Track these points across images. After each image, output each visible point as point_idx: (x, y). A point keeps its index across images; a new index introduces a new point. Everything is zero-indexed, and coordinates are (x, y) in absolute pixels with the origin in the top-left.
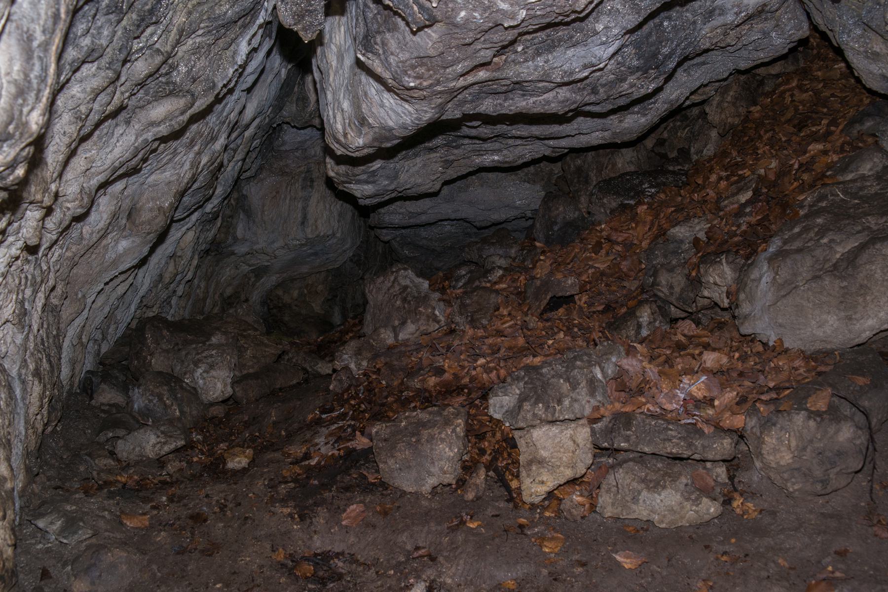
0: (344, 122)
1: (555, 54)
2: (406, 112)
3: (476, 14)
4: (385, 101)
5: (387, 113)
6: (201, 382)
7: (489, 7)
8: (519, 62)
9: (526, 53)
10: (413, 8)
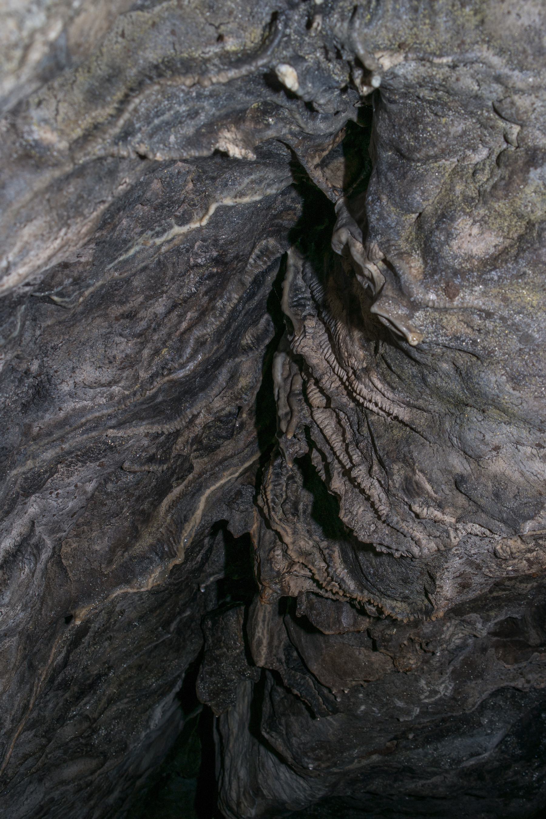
0: (239, 791)
1: (443, 743)
2: (300, 787)
3: (374, 709)
4: (281, 774)
5: (282, 786)
7: (386, 704)
8: (411, 749)
9: (416, 740)
10: (318, 699)
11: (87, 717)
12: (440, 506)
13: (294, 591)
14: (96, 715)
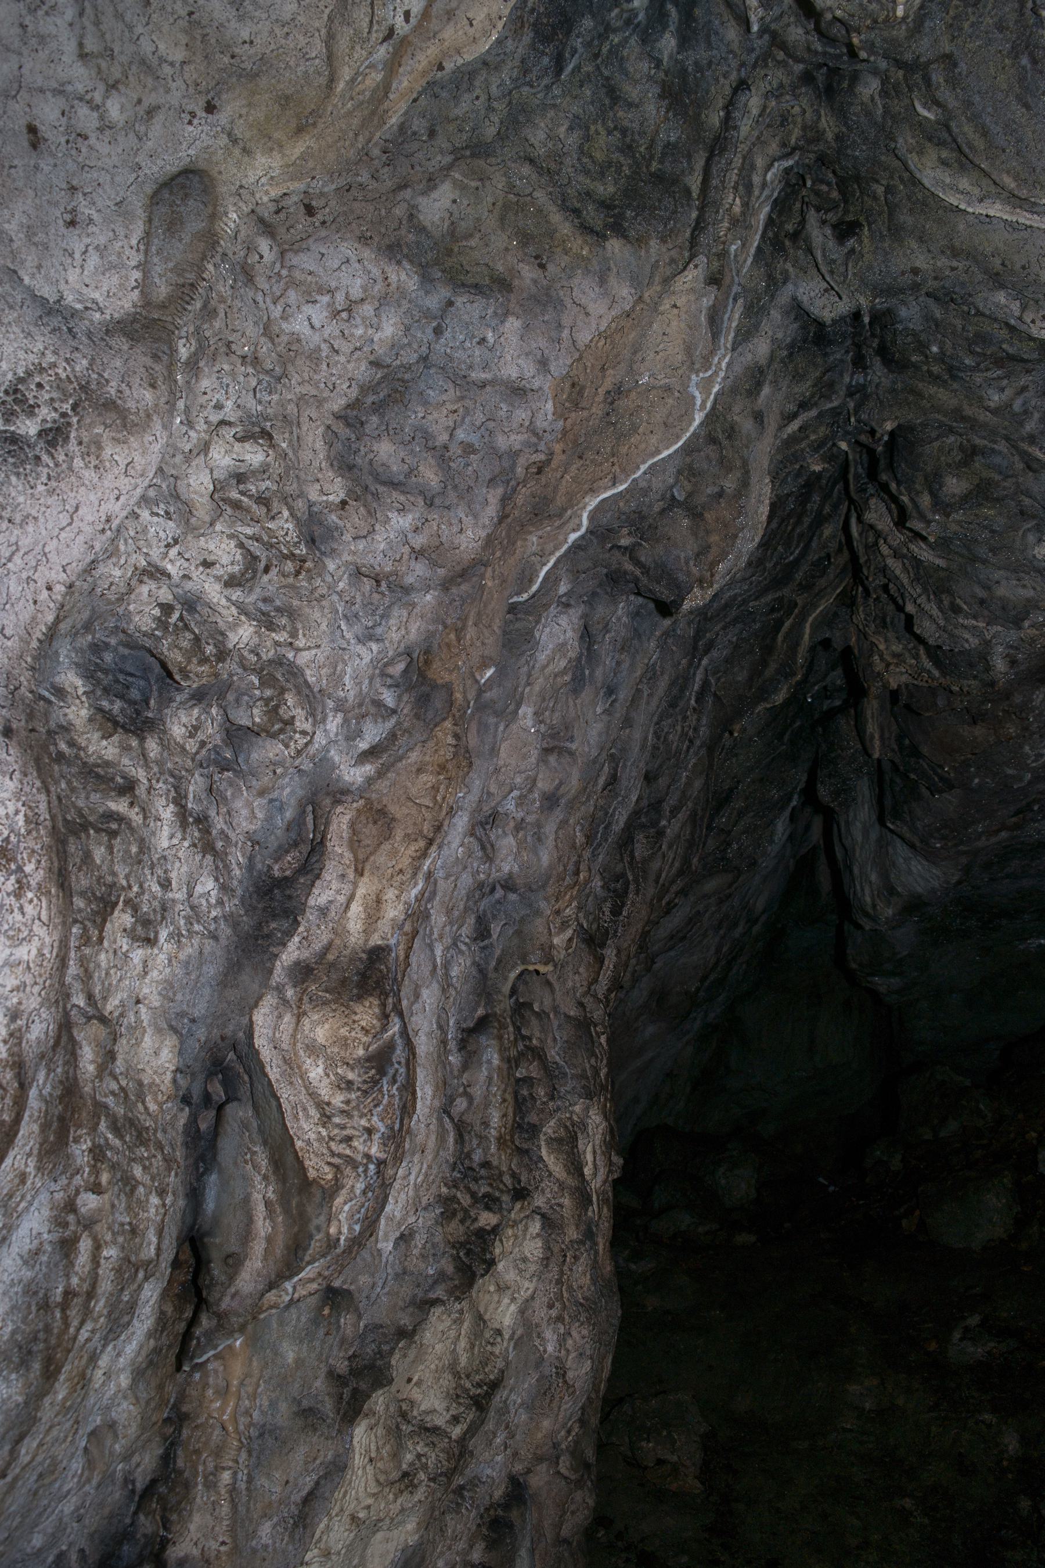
6: (723, 1182)
12: (975, 617)
13: (894, 685)
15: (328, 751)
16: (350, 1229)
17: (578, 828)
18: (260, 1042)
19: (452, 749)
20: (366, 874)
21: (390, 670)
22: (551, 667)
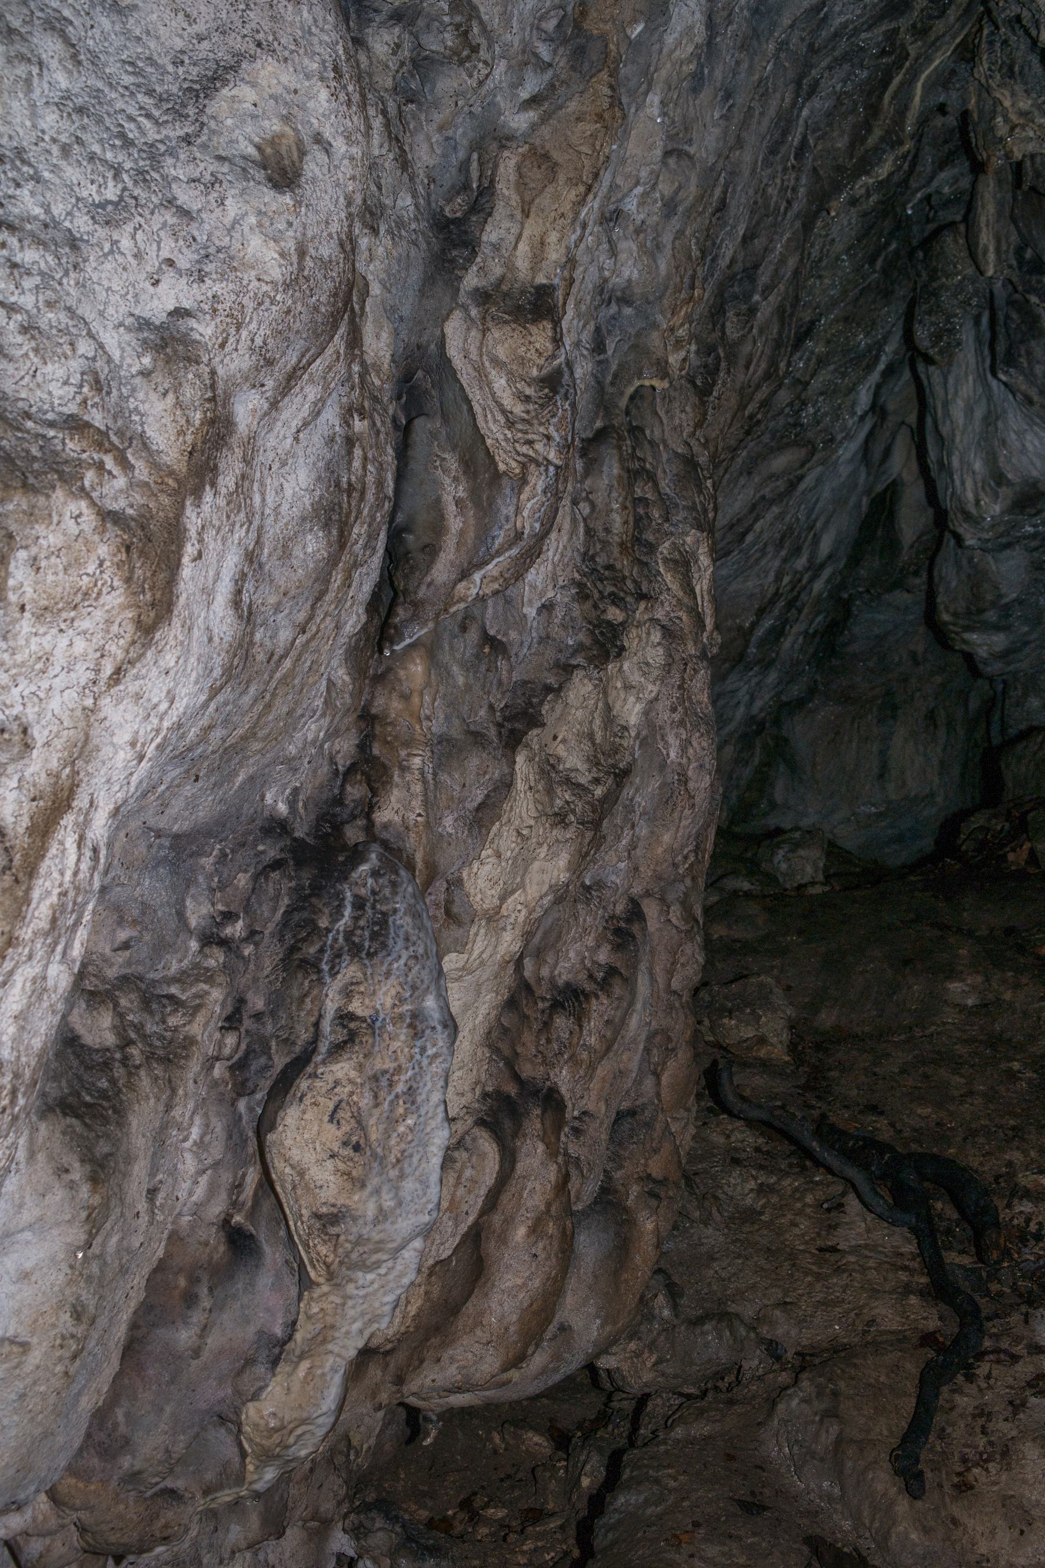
4: (1028, 445)
6: (784, 866)
11: (799, 380)
13: (1018, 155)
14: (807, 378)
15: (495, 96)
16: (532, 527)
17: (694, 241)
18: (453, 351)
19: (608, 100)
20: (532, 215)
21: (544, 25)
22: (678, 53)
